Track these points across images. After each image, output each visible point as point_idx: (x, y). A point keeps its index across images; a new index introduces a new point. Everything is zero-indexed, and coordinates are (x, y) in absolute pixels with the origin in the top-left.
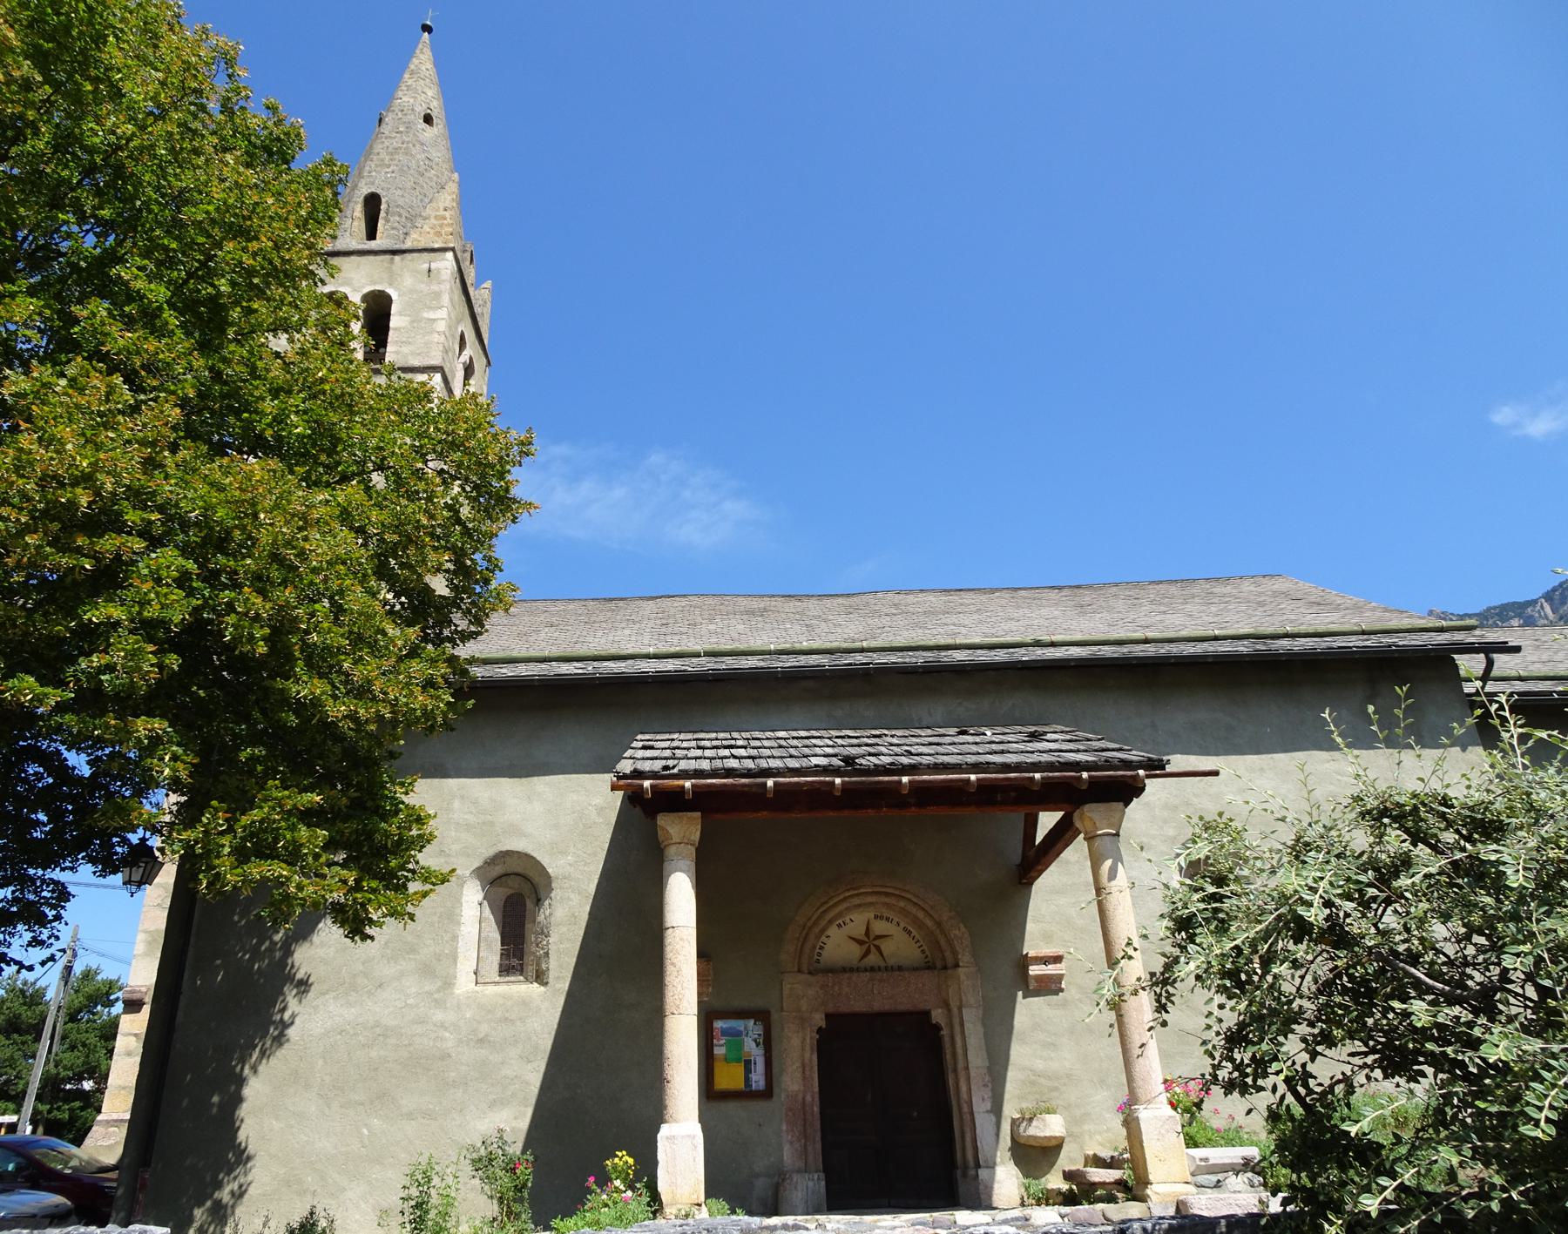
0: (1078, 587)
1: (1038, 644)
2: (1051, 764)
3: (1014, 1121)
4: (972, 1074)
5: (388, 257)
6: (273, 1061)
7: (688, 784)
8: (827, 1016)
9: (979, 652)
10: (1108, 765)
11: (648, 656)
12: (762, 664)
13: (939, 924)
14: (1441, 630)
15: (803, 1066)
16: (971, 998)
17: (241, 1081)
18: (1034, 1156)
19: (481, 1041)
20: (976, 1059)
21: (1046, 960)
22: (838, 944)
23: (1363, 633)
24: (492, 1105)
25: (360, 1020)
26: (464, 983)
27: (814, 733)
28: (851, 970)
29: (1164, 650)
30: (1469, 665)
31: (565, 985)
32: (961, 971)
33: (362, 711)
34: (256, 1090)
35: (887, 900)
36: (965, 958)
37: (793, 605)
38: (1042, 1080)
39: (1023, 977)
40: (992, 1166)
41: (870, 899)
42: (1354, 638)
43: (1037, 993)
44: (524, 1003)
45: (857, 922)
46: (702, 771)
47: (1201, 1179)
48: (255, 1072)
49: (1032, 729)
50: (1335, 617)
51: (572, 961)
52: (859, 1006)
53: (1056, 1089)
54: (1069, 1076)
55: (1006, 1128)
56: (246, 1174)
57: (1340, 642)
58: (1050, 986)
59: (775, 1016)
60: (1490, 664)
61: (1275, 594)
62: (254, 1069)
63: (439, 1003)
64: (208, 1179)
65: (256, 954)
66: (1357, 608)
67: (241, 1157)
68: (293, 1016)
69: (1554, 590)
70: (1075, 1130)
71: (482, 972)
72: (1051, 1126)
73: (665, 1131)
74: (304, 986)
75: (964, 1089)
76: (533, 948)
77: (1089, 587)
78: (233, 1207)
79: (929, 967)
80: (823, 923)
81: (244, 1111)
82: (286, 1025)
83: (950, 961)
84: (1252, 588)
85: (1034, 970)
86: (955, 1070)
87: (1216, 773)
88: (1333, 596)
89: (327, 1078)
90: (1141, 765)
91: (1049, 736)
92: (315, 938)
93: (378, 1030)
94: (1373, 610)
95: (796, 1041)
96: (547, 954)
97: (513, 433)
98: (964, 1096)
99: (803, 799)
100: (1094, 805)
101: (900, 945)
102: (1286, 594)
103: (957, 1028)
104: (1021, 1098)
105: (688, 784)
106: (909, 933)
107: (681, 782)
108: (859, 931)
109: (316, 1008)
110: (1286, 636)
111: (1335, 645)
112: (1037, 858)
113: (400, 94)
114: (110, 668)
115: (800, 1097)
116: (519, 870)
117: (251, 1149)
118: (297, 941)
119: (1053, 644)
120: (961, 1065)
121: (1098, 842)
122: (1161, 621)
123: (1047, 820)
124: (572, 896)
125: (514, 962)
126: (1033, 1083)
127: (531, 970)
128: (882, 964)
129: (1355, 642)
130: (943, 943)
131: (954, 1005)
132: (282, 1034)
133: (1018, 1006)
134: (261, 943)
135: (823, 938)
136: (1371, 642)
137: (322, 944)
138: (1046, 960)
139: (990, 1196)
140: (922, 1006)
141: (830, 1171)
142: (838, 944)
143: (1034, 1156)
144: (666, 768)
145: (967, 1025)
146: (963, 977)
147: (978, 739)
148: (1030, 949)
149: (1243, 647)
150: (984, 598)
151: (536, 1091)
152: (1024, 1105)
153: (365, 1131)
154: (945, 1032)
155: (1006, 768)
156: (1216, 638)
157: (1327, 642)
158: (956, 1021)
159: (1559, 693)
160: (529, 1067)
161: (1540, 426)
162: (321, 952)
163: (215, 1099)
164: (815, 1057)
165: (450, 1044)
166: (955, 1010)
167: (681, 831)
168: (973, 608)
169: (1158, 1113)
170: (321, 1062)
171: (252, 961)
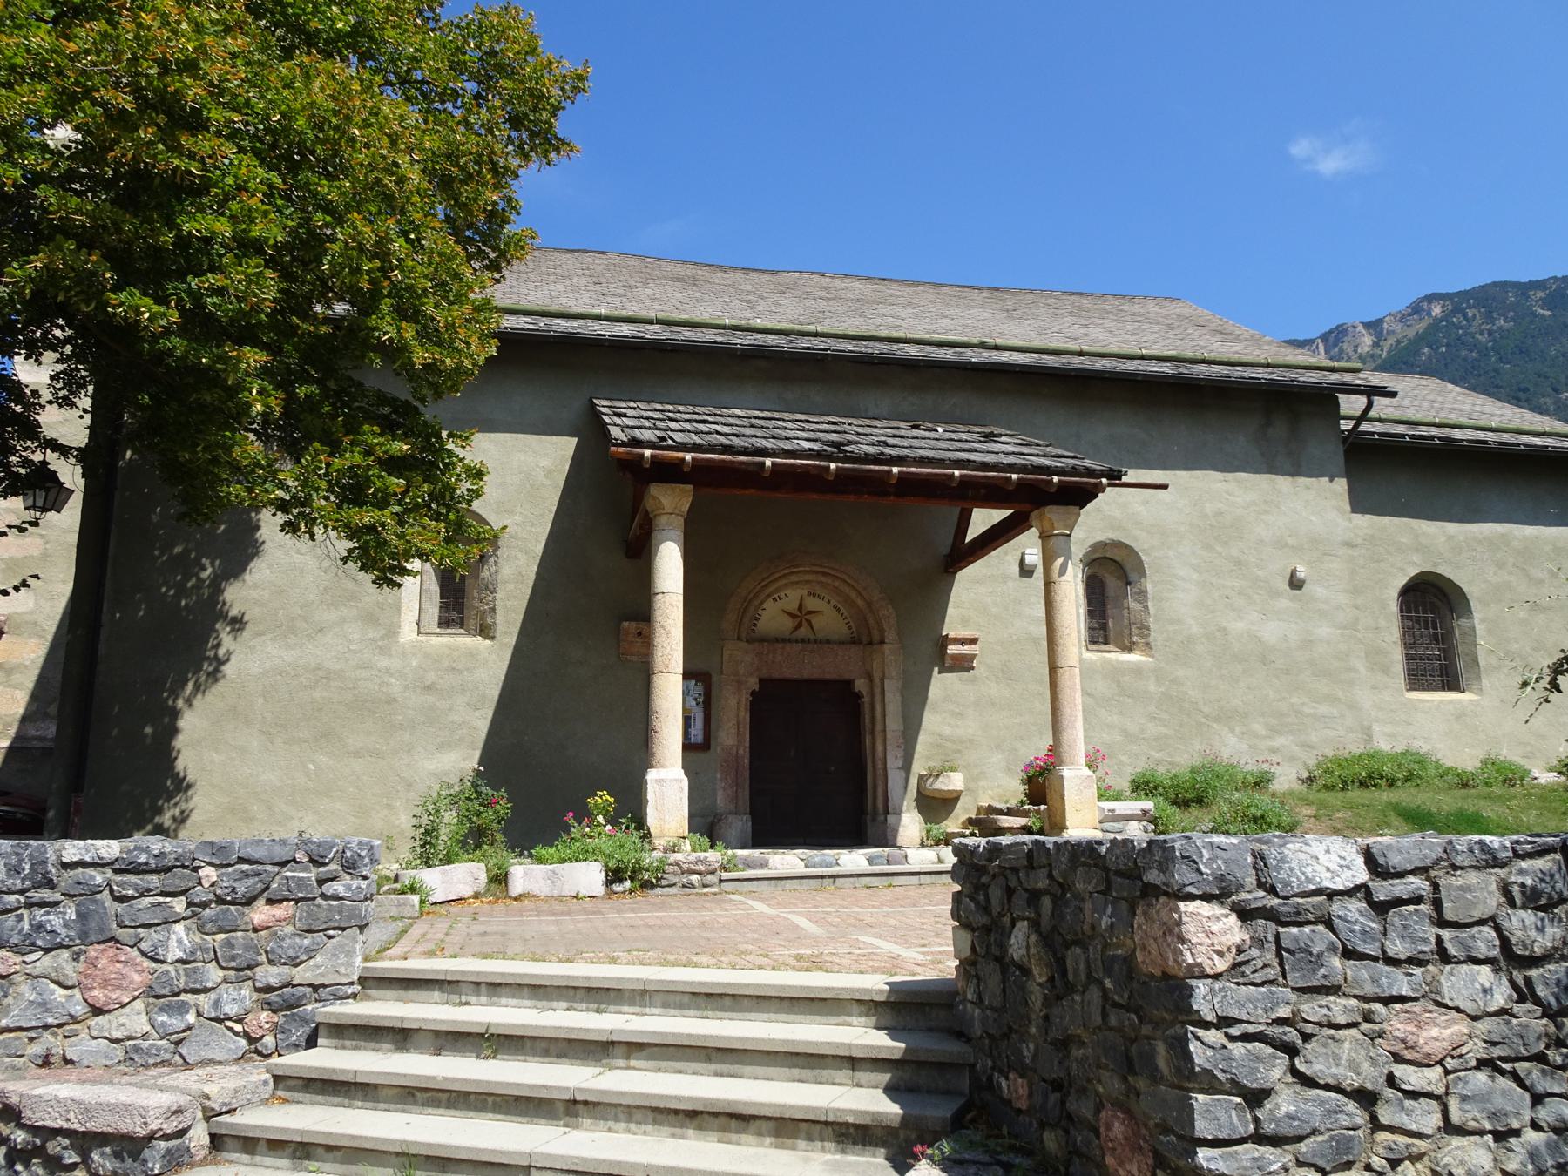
0: (997, 289)
1: (983, 346)
2: (1025, 466)
3: (921, 777)
6: (209, 696)
7: (688, 457)
8: (761, 681)
9: (929, 348)
10: (1074, 471)
12: (720, 339)
13: (869, 604)
14: (1332, 370)
16: (893, 671)
17: (175, 714)
18: (935, 806)
19: (428, 688)
20: (893, 724)
21: (963, 642)
22: (773, 616)
23: (1268, 366)
24: (441, 747)
25: (301, 662)
26: (408, 633)
27: (776, 415)
28: (784, 640)
29: (1099, 364)
30: (1351, 405)
31: (512, 640)
32: (886, 647)
33: (448, 361)
34: (190, 722)
35: (823, 579)
36: (891, 636)
37: (718, 276)
38: (948, 744)
39: (941, 655)
40: (898, 813)
41: (807, 577)
42: (1261, 370)
43: (951, 670)
44: (471, 654)
45: (791, 598)
46: (700, 446)
47: (1107, 826)
48: (190, 705)
49: (987, 430)
50: (1238, 347)
51: (518, 618)
52: (789, 673)
53: (959, 751)
54: (971, 741)
55: (913, 782)
56: (187, 801)
57: (1249, 373)
58: (963, 665)
59: (715, 679)
60: (1370, 405)
61: (1180, 318)
62: (189, 703)
63: (383, 651)
64: (147, 805)
65: (182, 591)
66: (1255, 341)
67: (182, 786)
68: (229, 653)
69: (1331, 332)
70: (972, 785)
71: (423, 623)
72: (954, 781)
73: (652, 775)
74: (238, 624)
75: (879, 748)
76: (476, 603)
77: (1007, 291)
78: (175, 830)
79: (855, 641)
80: (762, 597)
81: (179, 742)
82: (221, 662)
83: (876, 638)
84: (1156, 309)
85: (952, 650)
86: (873, 733)
87: (1165, 487)
88: (1230, 325)
89: (268, 716)
90: (1102, 474)
91: (1003, 439)
92: (247, 576)
93: (321, 673)
94: (1269, 343)
95: (733, 702)
96: (493, 610)
97: (565, 63)
98: (879, 753)
99: (797, 481)
100: (1054, 507)
101: (829, 620)
102: (1189, 319)
103: (878, 698)
104: (928, 758)
105: (688, 457)
107: (680, 455)
108: (793, 606)
109: (252, 648)
110: (1203, 361)
111: (1247, 375)
112: (964, 553)
114: (220, 292)
116: (1118, 559)
117: (190, 778)
118: (227, 580)
119: (996, 348)
120: (879, 727)
121: (1053, 541)
122: (1086, 335)
123: (983, 519)
124: (519, 555)
125: (454, 615)
126: (939, 746)
127: (472, 623)
128: (812, 637)
129: (1262, 374)
130: (871, 621)
131: (877, 676)
132: (217, 670)
133: (933, 681)
134: (186, 578)
136: (1276, 375)
137: (256, 586)
138: (963, 642)
139: (895, 837)
140: (847, 676)
141: (755, 814)
142: (773, 616)
143: (935, 806)
144: (663, 439)
145: (887, 694)
146: (887, 652)
147: (927, 434)
148: (951, 629)
149: (1167, 369)
150: (910, 290)
151: (484, 736)
152: (932, 764)
153: (312, 767)
154: (866, 700)
155: (985, 466)
156: (1143, 357)
157: (1238, 372)
158: (877, 690)
159: (1380, 434)
160: (477, 714)
161: (1331, 164)
162: (254, 594)
163: (148, 730)
165: (396, 689)
166: (877, 681)
167: (671, 502)
168: (903, 301)
169: (1078, 773)
170: (260, 700)
171: (178, 597)
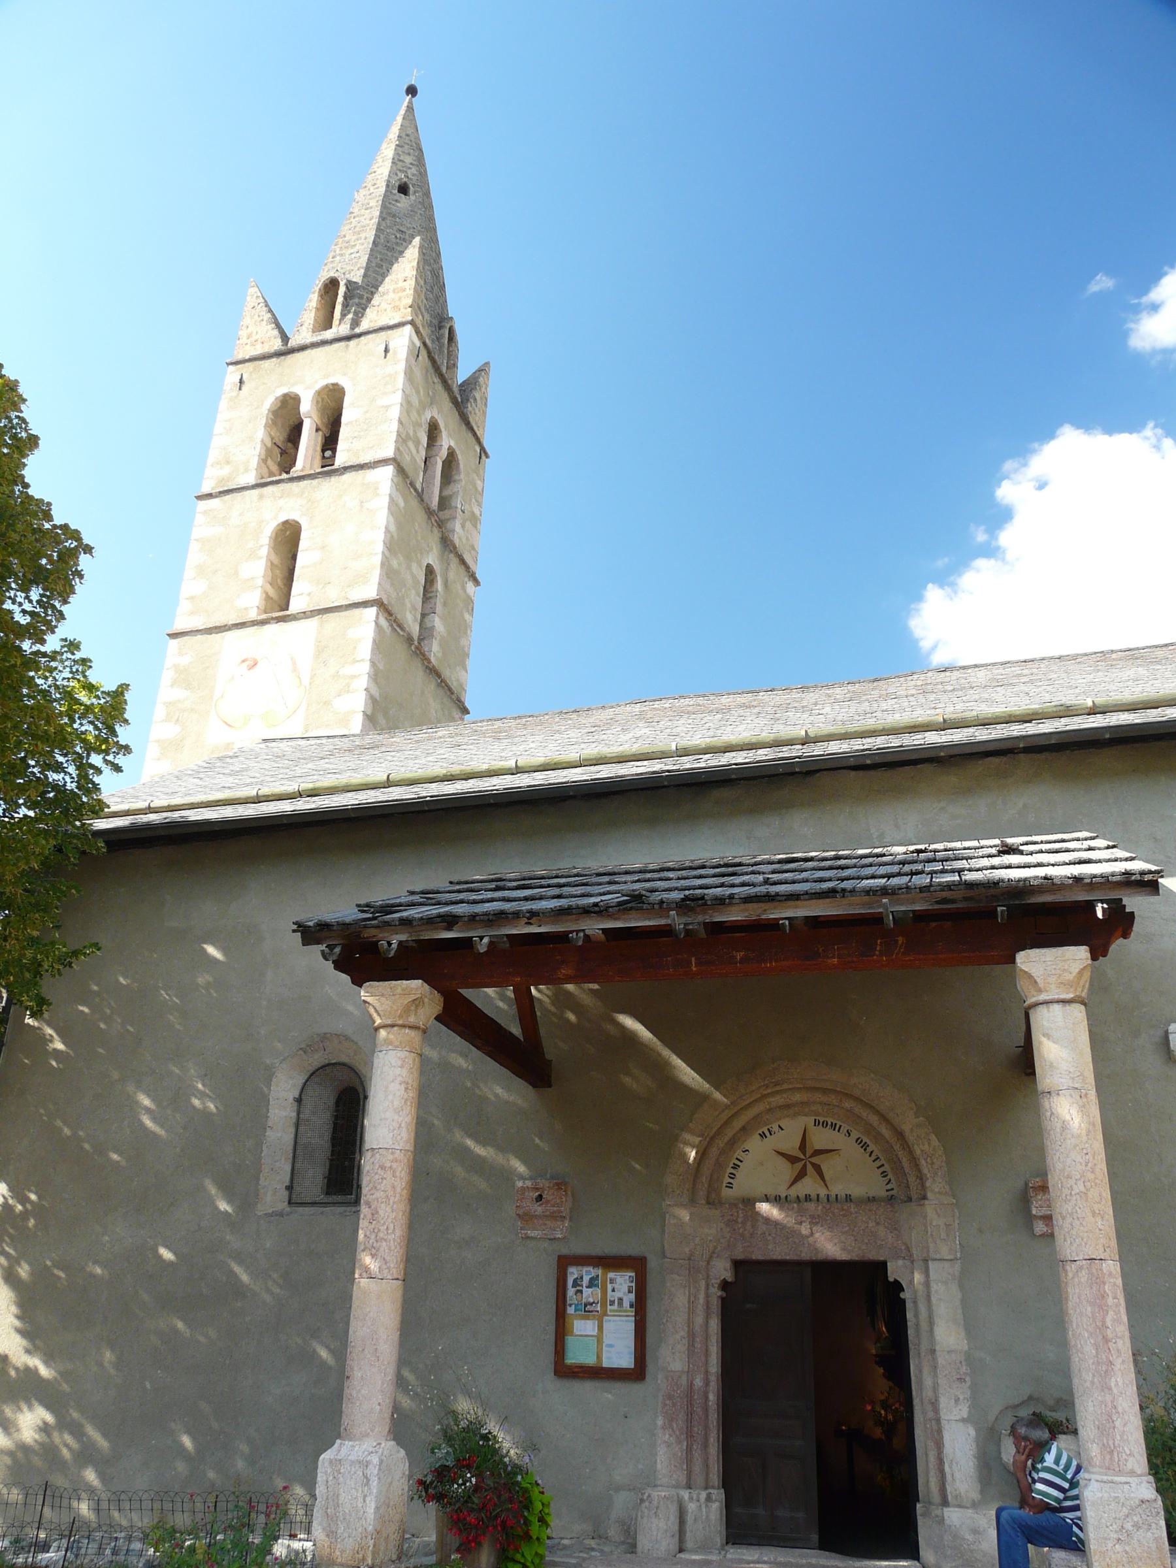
4: (941, 1361)
5: (343, 344)
11: (432, 780)
15: (691, 1335)
35: (825, 1099)
36: (936, 1186)
59: (653, 1263)
71: (297, 1188)
95: (681, 1299)
106: (865, 1146)
108: (791, 1144)
113: (375, 167)
115: (684, 1381)
135: (739, 1154)
140: (873, 1255)
164: (715, 1325)
